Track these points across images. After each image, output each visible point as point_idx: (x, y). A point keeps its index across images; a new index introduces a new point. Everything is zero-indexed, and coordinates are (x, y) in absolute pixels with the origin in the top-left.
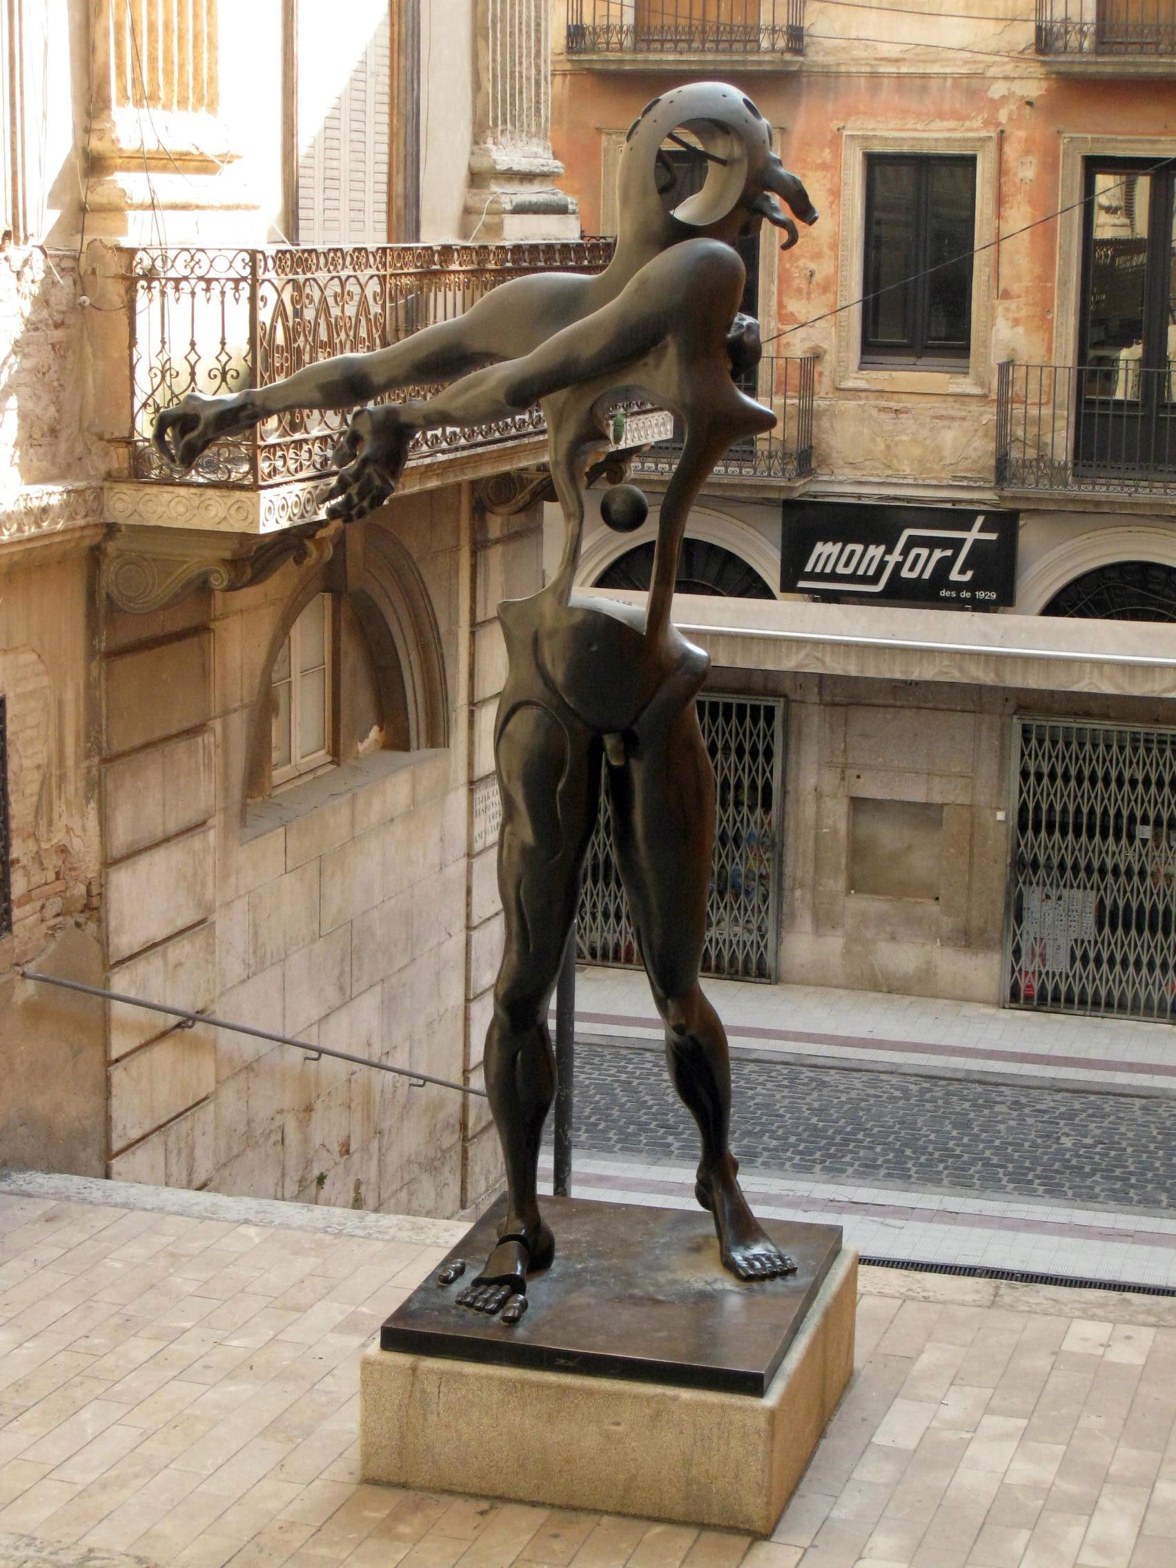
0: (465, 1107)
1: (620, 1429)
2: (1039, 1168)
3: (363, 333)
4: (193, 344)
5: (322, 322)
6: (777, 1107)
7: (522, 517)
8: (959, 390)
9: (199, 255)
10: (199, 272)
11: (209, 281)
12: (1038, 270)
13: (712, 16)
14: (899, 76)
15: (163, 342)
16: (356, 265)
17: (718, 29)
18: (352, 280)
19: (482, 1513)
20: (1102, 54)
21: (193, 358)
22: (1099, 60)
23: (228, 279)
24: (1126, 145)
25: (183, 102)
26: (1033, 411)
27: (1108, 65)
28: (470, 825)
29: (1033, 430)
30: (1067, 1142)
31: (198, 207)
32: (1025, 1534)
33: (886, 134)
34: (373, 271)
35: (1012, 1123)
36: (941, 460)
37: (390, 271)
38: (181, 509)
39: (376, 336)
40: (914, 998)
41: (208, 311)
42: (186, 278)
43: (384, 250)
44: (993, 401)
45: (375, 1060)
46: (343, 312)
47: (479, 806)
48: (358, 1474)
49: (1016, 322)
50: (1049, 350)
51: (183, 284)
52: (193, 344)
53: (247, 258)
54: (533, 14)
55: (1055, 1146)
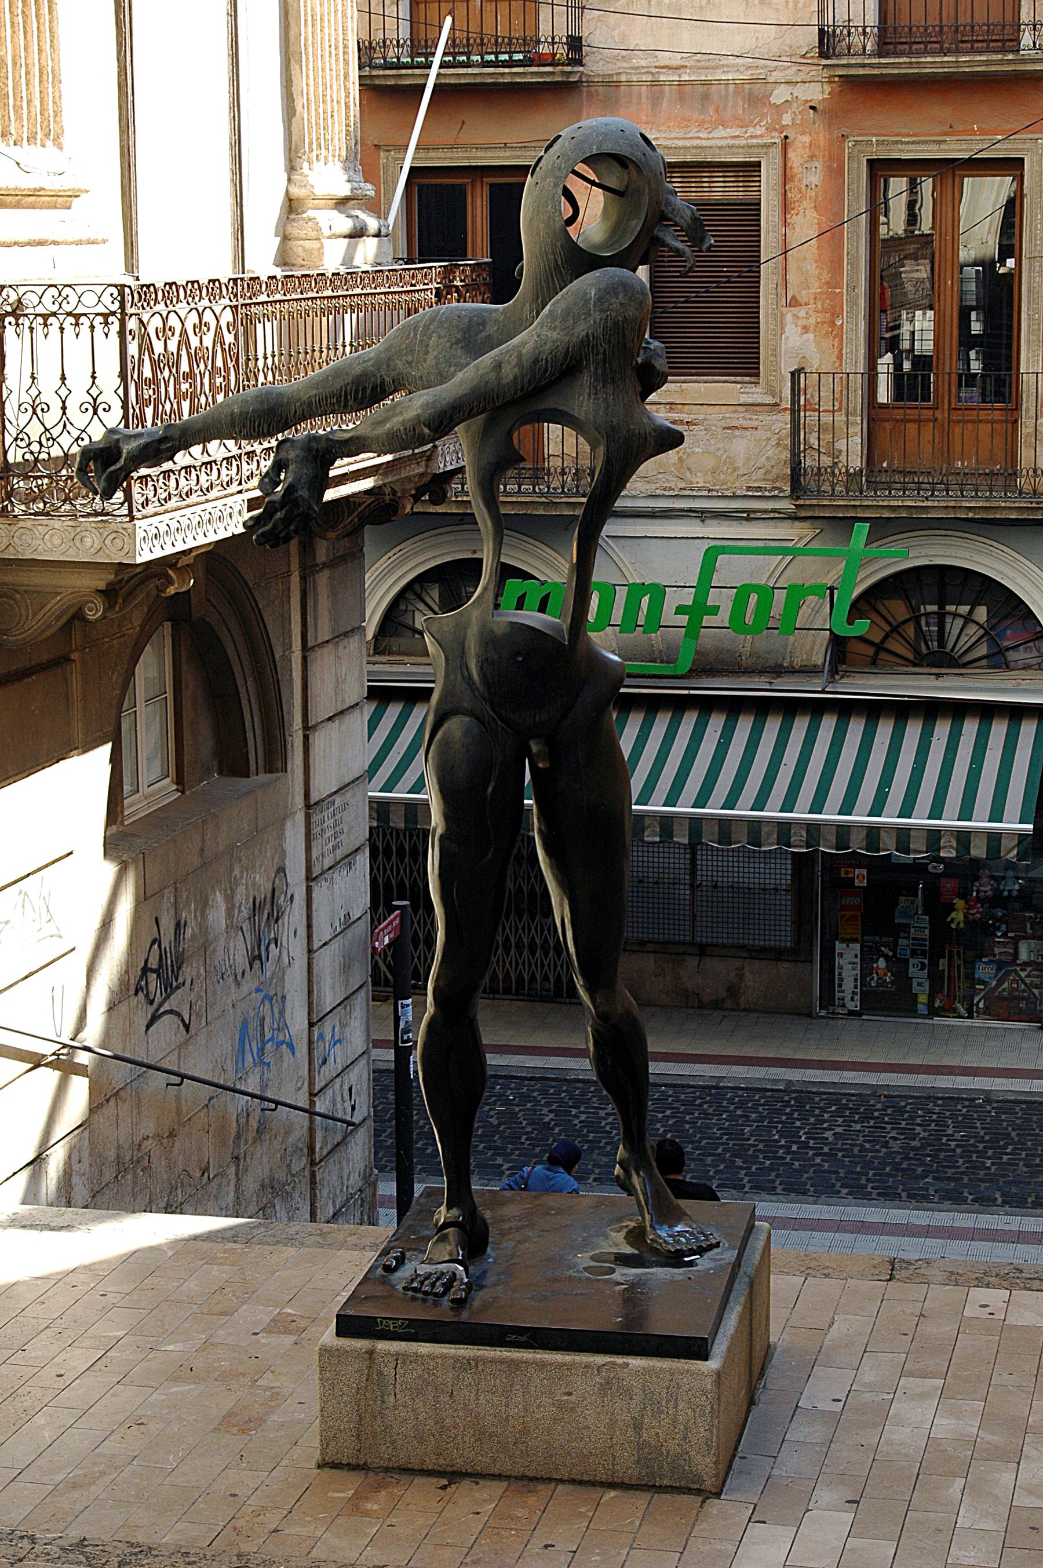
0: (311, 1130)
1: (573, 1398)
2: (871, 1173)
3: (219, 363)
4: (63, 378)
5: (184, 353)
6: (603, 1124)
7: (346, 542)
8: (750, 401)
9: (67, 291)
10: (68, 308)
11: (77, 317)
12: (826, 276)
13: (489, 29)
14: (681, 84)
15: (33, 378)
16: (212, 296)
17: (497, 41)
18: (208, 311)
19: (444, 1488)
20: (887, 55)
21: (63, 392)
22: (882, 61)
23: (97, 314)
24: (911, 147)
25: (31, 139)
26: (826, 418)
27: (899, 65)
28: (308, 849)
29: (827, 437)
30: (896, 1146)
31: (55, 243)
32: (959, 1482)
33: (669, 143)
34: (226, 302)
35: (839, 1130)
36: (735, 469)
37: (241, 301)
38: (57, 541)
39: (231, 365)
40: (726, 1013)
41: (77, 347)
42: (54, 314)
43: (235, 280)
44: (785, 409)
45: (229, 1084)
46: (201, 343)
47: (316, 830)
48: (317, 1456)
49: (806, 329)
50: (840, 357)
51: (51, 320)
52: (63, 378)
53: (116, 293)
54: (341, 37)
55: (884, 1150)
